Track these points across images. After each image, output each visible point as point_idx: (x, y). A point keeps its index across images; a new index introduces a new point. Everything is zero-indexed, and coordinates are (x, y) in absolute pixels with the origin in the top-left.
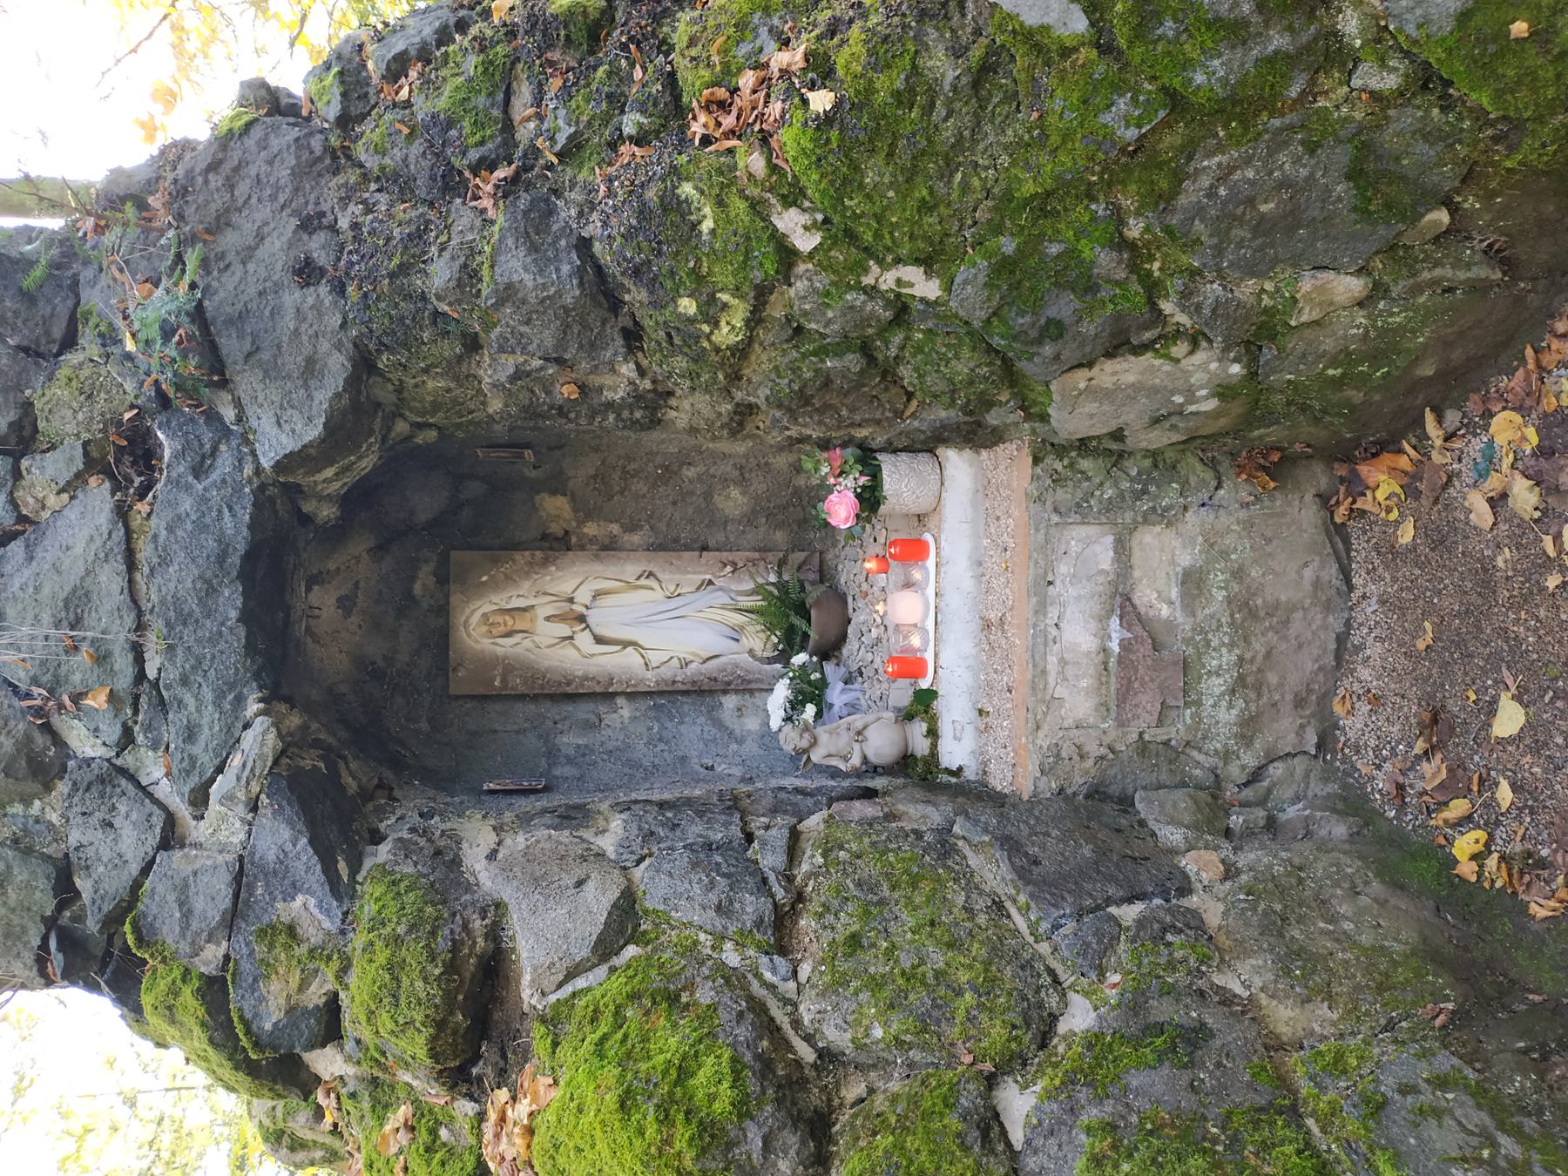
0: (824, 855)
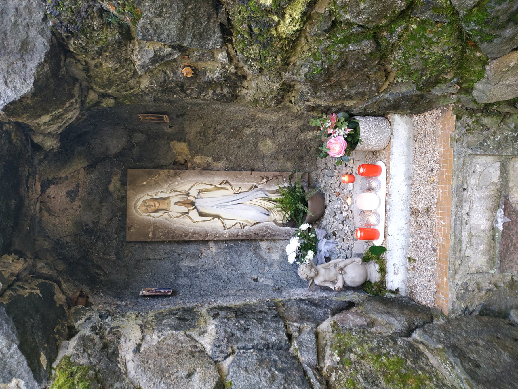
0: (340, 355)
